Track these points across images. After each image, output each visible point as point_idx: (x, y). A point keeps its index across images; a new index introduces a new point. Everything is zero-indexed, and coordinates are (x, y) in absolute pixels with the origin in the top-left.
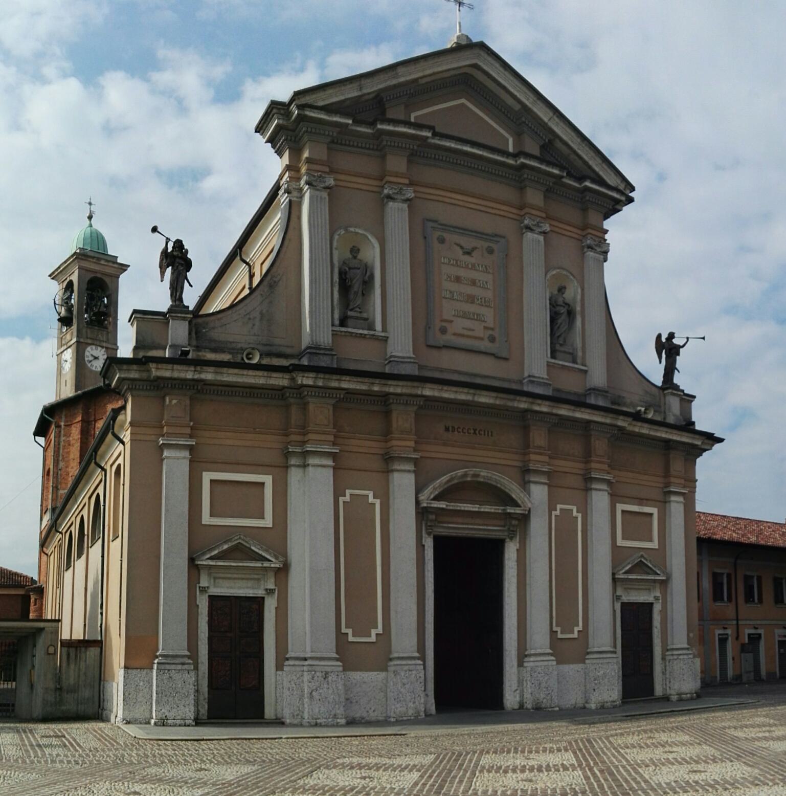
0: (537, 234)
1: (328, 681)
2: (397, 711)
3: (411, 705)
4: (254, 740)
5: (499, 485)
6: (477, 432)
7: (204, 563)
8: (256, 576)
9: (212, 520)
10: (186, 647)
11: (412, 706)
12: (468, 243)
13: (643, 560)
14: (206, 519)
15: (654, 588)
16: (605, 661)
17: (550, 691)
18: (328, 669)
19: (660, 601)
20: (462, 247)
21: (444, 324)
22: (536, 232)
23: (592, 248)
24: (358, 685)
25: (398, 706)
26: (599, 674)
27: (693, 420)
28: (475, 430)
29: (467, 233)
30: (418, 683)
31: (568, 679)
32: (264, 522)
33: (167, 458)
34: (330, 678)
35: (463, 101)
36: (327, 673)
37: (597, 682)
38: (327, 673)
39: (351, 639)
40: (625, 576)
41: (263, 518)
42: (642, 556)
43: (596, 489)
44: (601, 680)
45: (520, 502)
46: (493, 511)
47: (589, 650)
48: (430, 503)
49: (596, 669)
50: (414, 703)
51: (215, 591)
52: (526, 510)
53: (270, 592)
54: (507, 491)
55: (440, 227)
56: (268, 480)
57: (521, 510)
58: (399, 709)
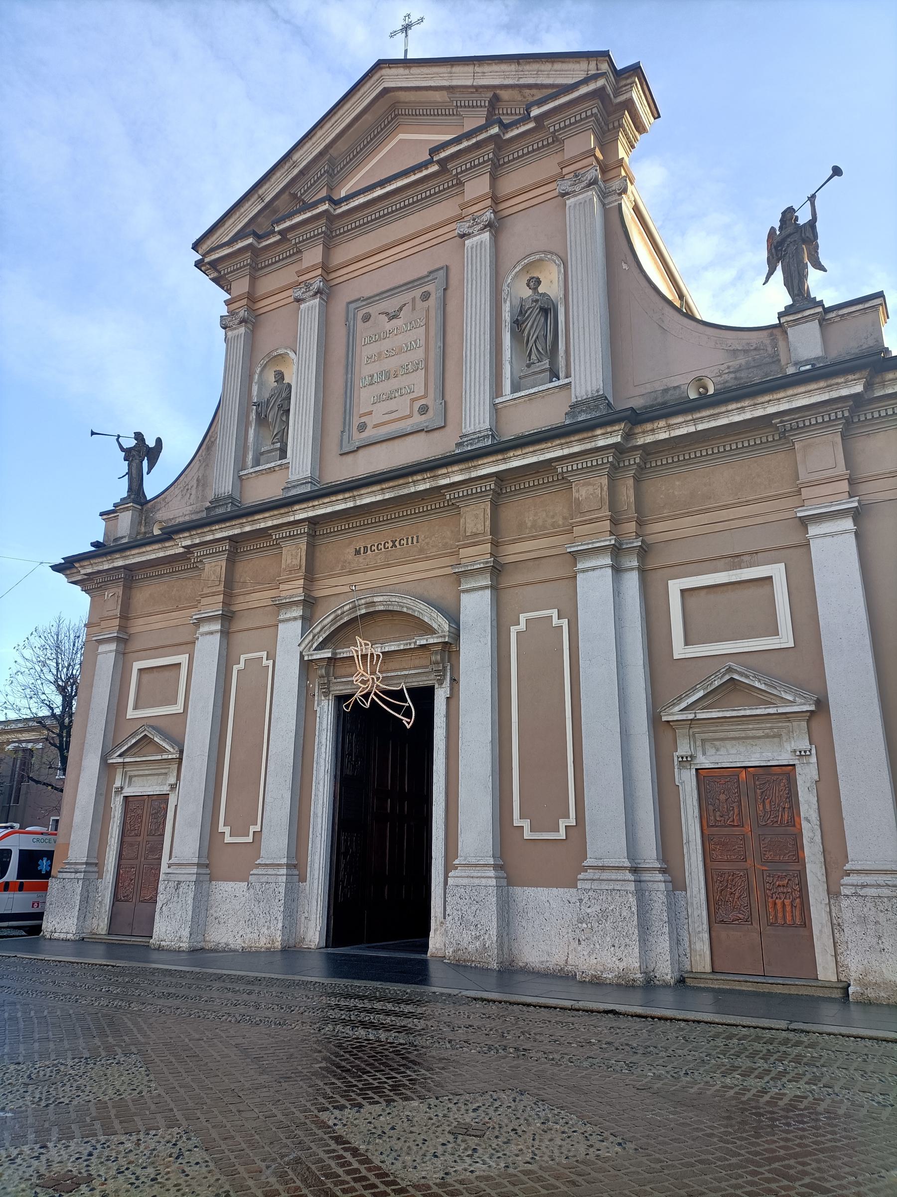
0: (479, 234)
1: (178, 894)
2: (246, 937)
3: (265, 930)
4: (869, 1043)
5: (405, 610)
6: (397, 543)
7: (675, 718)
8: (163, 771)
9: (687, 651)
10: (626, 855)
11: (266, 932)
12: (390, 305)
13: (736, 677)
14: (680, 650)
15: (790, 732)
16: (605, 886)
17: (482, 932)
18: (181, 878)
19: (814, 759)
20: (387, 314)
21: (363, 420)
22: (476, 233)
23: (567, 194)
24: (228, 901)
25: (248, 931)
26: (589, 911)
27: (886, 346)
28: (394, 542)
29: (416, 284)
30: (277, 901)
31: (547, 915)
32: (777, 641)
33: (816, 537)
34: (181, 889)
35: (401, 136)
36: (179, 883)
37: (584, 925)
38: (179, 883)
39: (228, 839)
40: (120, 760)
41: (777, 633)
42: (730, 670)
43: (584, 571)
44: (596, 925)
45: (435, 626)
46: (402, 647)
47: (847, 867)
48: (311, 655)
49: (581, 900)
50: (269, 928)
51: (704, 761)
52: (444, 636)
53: (802, 755)
54: (416, 614)
55: (364, 303)
56: (777, 571)
57: (437, 637)
58: (249, 935)
